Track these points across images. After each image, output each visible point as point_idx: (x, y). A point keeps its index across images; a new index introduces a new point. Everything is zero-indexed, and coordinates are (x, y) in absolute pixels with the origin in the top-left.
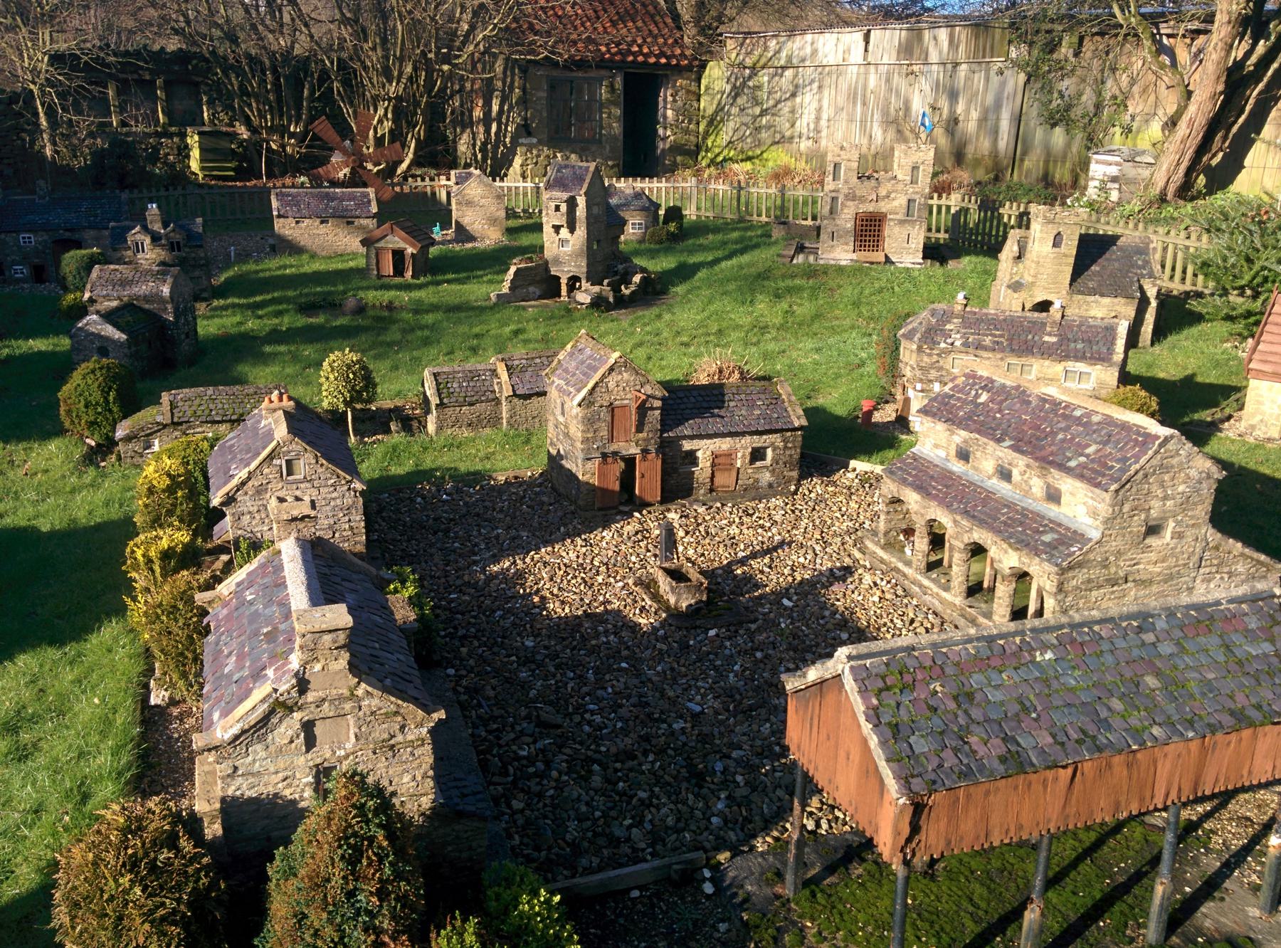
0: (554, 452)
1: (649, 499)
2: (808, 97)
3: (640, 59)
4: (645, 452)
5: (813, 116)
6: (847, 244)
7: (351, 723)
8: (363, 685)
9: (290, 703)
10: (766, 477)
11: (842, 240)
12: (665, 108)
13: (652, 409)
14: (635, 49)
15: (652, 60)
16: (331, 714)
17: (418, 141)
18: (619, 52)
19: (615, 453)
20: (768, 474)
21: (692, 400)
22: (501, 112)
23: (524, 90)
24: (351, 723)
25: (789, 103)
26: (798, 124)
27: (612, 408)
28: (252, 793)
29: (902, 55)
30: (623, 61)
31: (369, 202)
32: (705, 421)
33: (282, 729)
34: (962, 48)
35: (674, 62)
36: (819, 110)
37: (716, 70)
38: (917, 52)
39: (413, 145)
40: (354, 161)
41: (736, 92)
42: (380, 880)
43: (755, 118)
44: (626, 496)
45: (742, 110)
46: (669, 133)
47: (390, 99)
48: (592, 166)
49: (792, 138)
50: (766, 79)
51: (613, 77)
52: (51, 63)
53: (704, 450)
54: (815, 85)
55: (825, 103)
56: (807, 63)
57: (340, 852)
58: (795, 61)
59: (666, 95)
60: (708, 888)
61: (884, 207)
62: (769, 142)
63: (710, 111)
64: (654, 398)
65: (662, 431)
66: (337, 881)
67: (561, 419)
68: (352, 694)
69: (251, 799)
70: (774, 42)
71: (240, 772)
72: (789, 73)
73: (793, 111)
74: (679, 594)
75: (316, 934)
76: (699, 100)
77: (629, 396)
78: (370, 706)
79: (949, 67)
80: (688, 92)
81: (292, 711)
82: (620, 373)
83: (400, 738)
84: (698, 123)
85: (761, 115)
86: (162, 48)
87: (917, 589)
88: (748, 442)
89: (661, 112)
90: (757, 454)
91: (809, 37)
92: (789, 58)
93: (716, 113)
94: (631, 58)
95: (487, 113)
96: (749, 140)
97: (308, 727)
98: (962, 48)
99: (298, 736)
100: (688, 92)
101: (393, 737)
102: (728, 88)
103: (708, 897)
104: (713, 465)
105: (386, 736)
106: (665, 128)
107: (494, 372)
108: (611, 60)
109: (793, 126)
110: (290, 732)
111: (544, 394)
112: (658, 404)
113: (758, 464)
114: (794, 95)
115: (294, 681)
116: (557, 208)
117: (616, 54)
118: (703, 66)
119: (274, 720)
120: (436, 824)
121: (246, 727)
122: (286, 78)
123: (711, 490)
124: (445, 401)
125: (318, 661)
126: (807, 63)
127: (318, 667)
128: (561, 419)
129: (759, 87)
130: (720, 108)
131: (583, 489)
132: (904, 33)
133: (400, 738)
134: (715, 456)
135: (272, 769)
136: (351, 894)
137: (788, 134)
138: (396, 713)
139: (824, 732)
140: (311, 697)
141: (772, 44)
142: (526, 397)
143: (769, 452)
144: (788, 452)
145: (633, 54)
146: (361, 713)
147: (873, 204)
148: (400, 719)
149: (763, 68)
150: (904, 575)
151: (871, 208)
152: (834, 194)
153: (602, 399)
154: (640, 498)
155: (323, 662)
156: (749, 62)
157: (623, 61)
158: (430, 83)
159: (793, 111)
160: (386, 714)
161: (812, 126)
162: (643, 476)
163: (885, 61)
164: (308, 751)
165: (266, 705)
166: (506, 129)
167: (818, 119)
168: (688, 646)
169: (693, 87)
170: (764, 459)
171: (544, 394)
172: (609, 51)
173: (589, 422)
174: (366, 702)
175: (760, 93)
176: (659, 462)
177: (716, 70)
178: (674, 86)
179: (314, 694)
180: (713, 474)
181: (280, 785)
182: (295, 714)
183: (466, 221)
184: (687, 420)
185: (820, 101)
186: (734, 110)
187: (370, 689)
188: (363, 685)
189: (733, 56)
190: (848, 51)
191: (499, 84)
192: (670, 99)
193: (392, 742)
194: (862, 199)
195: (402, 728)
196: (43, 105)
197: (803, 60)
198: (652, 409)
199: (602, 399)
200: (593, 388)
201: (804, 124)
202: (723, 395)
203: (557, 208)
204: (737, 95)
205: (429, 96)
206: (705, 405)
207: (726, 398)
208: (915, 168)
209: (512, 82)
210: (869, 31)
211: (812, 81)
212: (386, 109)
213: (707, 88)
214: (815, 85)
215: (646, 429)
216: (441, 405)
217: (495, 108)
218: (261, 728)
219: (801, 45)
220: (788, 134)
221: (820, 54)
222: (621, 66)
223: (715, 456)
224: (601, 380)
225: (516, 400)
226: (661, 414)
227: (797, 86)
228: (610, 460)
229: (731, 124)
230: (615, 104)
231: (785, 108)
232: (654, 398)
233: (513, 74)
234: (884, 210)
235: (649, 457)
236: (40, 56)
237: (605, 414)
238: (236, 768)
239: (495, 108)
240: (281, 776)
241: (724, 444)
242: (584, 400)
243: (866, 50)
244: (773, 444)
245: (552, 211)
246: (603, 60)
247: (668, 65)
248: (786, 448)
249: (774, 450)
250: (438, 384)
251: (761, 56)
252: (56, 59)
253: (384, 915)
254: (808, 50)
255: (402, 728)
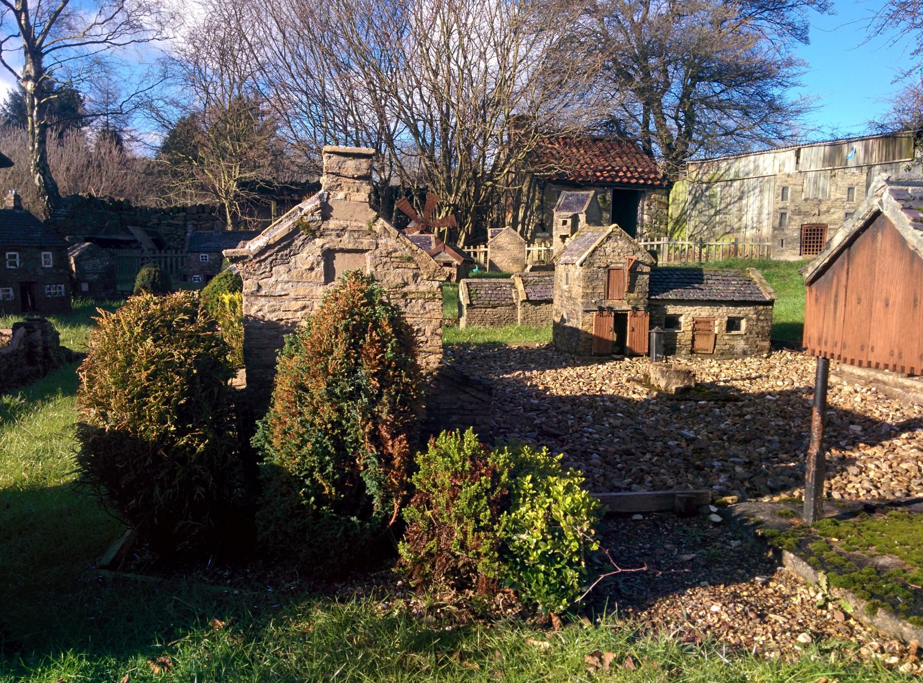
0: (557, 320)
1: (637, 350)
2: (752, 199)
3: (625, 180)
4: (635, 309)
5: (756, 212)
6: (794, 249)
7: (368, 261)
8: (381, 220)
9: (313, 226)
10: (741, 345)
11: (790, 246)
12: (643, 214)
13: (642, 273)
14: (621, 174)
15: (634, 181)
16: (350, 246)
17: (467, 234)
18: (610, 176)
19: (610, 309)
20: (742, 342)
21: (675, 276)
22: (525, 217)
23: (541, 201)
24: (368, 261)
25: (737, 205)
26: (744, 218)
27: (608, 269)
28: (273, 317)
29: (827, 164)
30: (613, 182)
31: (430, 243)
32: (687, 291)
33: (304, 254)
34: (875, 154)
35: (650, 182)
36: (761, 207)
37: (681, 187)
38: (838, 162)
39: (463, 237)
40: (423, 227)
41: (696, 201)
42: (381, 362)
43: (710, 217)
44: (618, 348)
45: (700, 212)
46: (645, 231)
47: (450, 205)
48: (592, 193)
49: (740, 228)
50: (719, 189)
51: (605, 192)
52: (238, 187)
53: (687, 315)
54: (757, 190)
55: (766, 202)
56: (751, 175)
57: (344, 322)
58: (741, 175)
59: (643, 205)
60: (716, 518)
61: (824, 219)
62: (721, 233)
63: (675, 216)
64: (644, 264)
65: (651, 293)
66: (339, 352)
67: (565, 287)
68: (371, 229)
69: (270, 322)
70: (725, 163)
71: (263, 293)
72: (736, 184)
73: (740, 210)
74: (669, 378)
75: (315, 412)
76: (667, 209)
77: (623, 261)
78: (386, 245)
79: (865, 169)
80: (660, 203)
81: (315, 237)
82: (616, 241)
83: (412, 287)
84: (667, 224)
85: (715, 215)
86: (307, 181)
87: (899, 390)
88: (725, 313)
89: (639, 216)
90: (732, 324)
91: (752, 158)
92: (737, 174)
93: (681, 215)
94: (618, 180)
95: (515, 217)
96: (706, 233)
97: (328, 255)
98: (875, 154)
99: (318, 264)
100: (660, 203)
101: (406, 284)
102: (690, 198)
103: (716, 524)
104: (694, 330)
105: (400, 281)
106: (642, 226)
107: (513, 285)
108: (603, 181)
109: (740, 220)
110: (311, 258)
111: (550, 302)
112: (647, 269)
113: (733, 332)
114: (741, 198)
115: (318, 202)
116: (565, 223)
117: (607, 177)
118: (670, 185)
119: (298, 242)
120: (442, 387)
121: (272, 242)
122: (383, 199)
123: (692, 352)
124: (474, 302)
125: (342, 189)
126: (751, 175)
127: (341, 195)
128: (565, 287)
129: (714, 196)
130: (684, 213)
131: (582, 337)
132: (827, 148)
133: (412, 287)
134: (696, 322)
135: (292, 295)
136: (352, 372)
137: (736, 226)
138: (410, 259)
139: (853, 299)
140: (332, 224)
141: (724, 165)
142: (537, 303)
143: (743, 323)
144: (760, 324)
145: (620, 177)
146: (377, 252)
147: (816, 217)
148: (413, 266)
149: (716, 182)
150: (885, 383)
151: (814, 220)
152: (783, 211)
153: (600, 261)
154: (630, 349)
155: (345, 191)
156: (705, 179)
157: (613, 182)
158: (477, 192)
159: (740, 210)
160: (401, 257)
161: (755, 219)
162: (633, 330)
163: (813, 168)
164: (326, 283)
165: (291, 222)
166: (528, 228)
167: (760, 214)
168: (679, 409)
169: (664, 199)
170: (739, 329)
171: (550, 302)
172: (602, 175)
173: (589, 280)
174: (383, 241)
175: (714, 200)
176: (648, 319)
177: (681, 187)
178: (649, 199)
179: (336, 222)
180: (693, 337)
181: (299, 314)
182: (317, 240)
183: (496, 261)
184: (672, 289)
185: (761, 201)
186: (694, 213)
187: (387, 225)
188: (381, 220)
189: (695, 174)
190: (783, 164)
191: (525, 199)
192: (646, 207)
193: (405, 289)
194: (806, 214)
195: (416, 276)
196: (230, 212)
197: (747, 174)
198: (642, 273)
199: (600, 261)
200: (593, 251)
201: (747, 219)
202: (703, 275)
203: (565, 223)
204: (696, 202)
205: (476, 203)
206: (686, 280)
207: (705, 277)
208: (850, 189)
209: (534, 195)
210: (799, 149)
211: (755, 188)
212: (447, 213)
213: (674, 200)
214: (757, 190)
215: (637, 290)
216: (470, 306)
217: (521, 215)
218: (285, 248)
219: (744, 165)
220: (736, 226)
221: (761, 168)
222: (611, 185)
223: (696, 322)
224: (600, 245)
225: (528, 305)
226: (650, 278)
227: (743, 193)
228: (605, 313)
229: (692, 223)
230: (607, 210)
231: (734, 209)
232: (644, 264)
233: (534, 191)
234: (825, 222)
235: (639, 313)
236: (231, 182)
237: (602, 274)
238: (260, 287)
239: (521, 215)
240: (300, 304)
241: (704, 312)
242: (585, 260)
243: (797, 163)
244: (747, 315)
245: (560, 225)
246: (598, 181)
247: (645, 184)
248: (758, 320)
249: (747, 321)
250: (469, 291)
251: (714, 174)
252: (242, 184)
253: (384, 405)
254: (752, 166)
255: (416, 276)
